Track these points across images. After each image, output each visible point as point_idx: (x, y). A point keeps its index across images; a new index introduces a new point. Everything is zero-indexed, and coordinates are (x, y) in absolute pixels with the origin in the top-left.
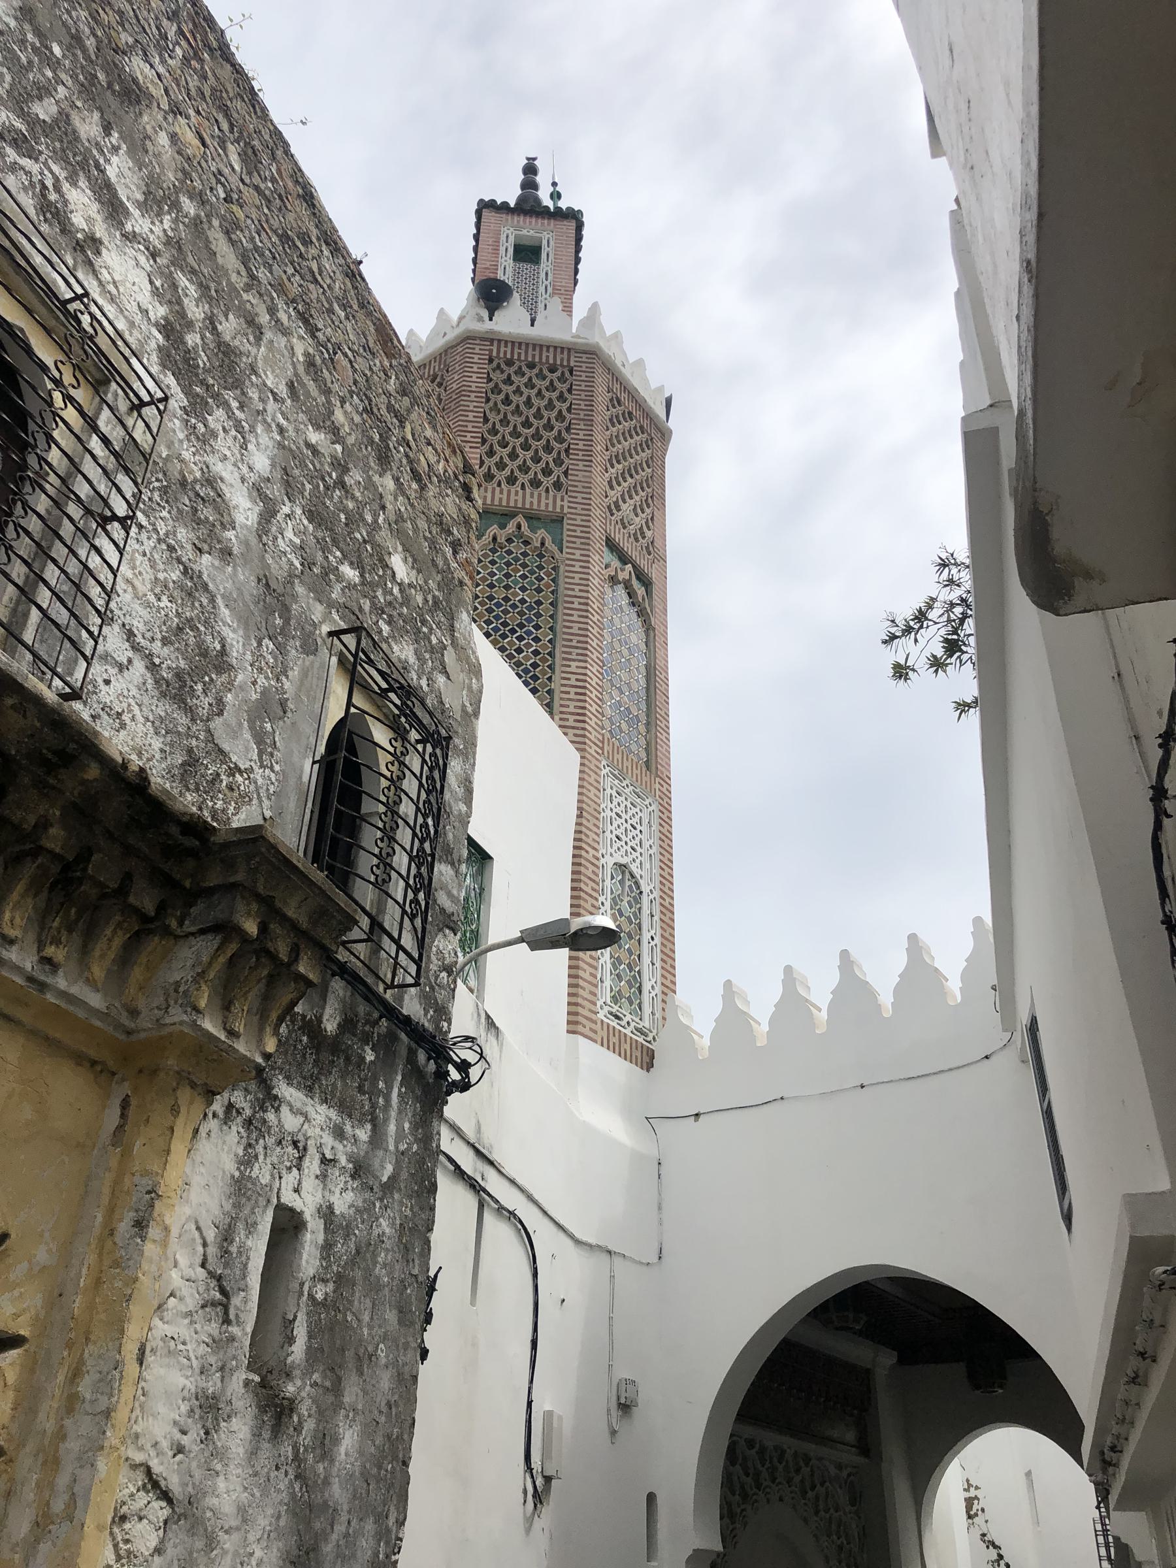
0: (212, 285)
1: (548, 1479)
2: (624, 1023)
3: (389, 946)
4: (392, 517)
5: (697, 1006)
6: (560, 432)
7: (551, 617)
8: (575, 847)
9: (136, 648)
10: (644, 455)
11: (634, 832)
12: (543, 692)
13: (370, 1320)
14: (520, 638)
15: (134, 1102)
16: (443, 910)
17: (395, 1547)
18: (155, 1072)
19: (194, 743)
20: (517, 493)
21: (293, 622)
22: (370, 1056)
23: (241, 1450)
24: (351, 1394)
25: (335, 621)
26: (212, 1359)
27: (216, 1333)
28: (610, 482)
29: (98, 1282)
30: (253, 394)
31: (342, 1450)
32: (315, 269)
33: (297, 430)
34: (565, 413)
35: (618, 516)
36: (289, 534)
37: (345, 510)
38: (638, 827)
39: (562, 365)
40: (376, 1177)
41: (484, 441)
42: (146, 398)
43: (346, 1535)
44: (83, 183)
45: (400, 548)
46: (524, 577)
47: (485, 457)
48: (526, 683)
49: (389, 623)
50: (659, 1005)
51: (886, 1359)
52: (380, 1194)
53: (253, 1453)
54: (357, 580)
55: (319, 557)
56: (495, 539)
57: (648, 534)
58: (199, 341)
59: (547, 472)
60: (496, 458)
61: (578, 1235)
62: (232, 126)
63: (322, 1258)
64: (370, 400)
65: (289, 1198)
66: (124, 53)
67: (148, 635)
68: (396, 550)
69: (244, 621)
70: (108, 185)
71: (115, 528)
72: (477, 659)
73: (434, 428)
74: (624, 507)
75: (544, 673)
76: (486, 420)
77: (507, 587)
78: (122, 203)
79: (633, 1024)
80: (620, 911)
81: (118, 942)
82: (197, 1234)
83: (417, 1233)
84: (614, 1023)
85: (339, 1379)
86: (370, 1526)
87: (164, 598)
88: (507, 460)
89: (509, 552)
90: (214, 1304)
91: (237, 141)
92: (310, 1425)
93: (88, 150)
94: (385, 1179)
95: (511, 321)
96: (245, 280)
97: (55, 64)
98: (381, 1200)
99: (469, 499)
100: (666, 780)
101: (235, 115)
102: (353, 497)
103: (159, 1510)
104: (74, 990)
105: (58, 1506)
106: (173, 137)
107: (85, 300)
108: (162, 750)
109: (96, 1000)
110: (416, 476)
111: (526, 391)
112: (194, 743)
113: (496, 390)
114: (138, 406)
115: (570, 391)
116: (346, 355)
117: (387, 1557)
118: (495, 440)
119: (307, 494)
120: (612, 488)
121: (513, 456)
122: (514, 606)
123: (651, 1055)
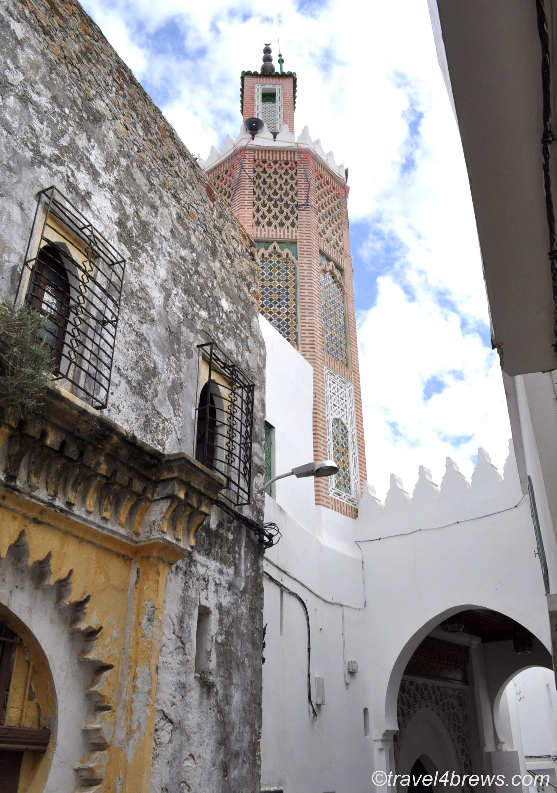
0: (136, 195)
1: (319, 706)
2: (342, 497)
3: (234, 488)
4: (220, 281)
5: (378, 486)
6: (292, 196)
7: (294, 294)
8: (314, 413)
9: (121, 375)
10: (336, 202)
11: (342, 401)
12: (292, 336)
13: (240, 648)
14: (279, 307)
15: (141, 571)
16: (256, 465)
17: (259, 736)
18: (148, 558)
19: (147, 412)
20: (272, 231)
21: (182, 345)
22: (231, 537)
23: (196, 703)
24: (236, 679)
25: (199, 339)
26: (182, 669)
27: (181, 659)
28: (319, 220)
29: (137, 643)
30: (156, 241)
31: (234, 701)
32: (178, 170)
33: (176, 252)
34: (294, 186)
35: (324, 237)
36: (177, 303)
37: (199, 284)
38: (344, 398)
39: (291, 161)
40: (238, 589)
41: (254, 204)
42: (115, 261)
43: (239, 732)
44: (82, 168)
45: (224, 295)
46: (279, 274)
47: (255, 213)
48: (284, 336)
49: (222, 333)
50: (359, 486)
51: (475, 642)
52: (240, 596)
53: (201, 704)
54: (207, 316)
55: (190, 310)
56: (263, 255)
57: (341, 244)
58: (132, 224)
59: (287, 218)
60: (261, 213)
61: (326, 599)
62: (137, 115)
63: (219, 625)
64: (206, 226)
65: (204, 602)
66: (92, 100)
67: (126, 368)
68: (223, 297)
69: (161, 350)
70: (92, 166)
71: (109, 326)
72: (263, 339)
73: (235, 229)
74: (327, 232)
75: (292, 324)
76: (254, 193)
77: (271, 280)
78: (97, 171)
79: (347, 497)
80: (337, 442)
81: (130, 505)
82: (170, 620)
83: (256, 611)
84: (337, 498)
85: (231, 674)
86: (248, 729)
87: (130, 349)
88: (266, 213)
89: (271, 262)
90: (179, 648)
91: (140, 121)
92: (221, 692)
93: (83, 152)
94: (241, 589)
95: (264, 139)
96: (149, 187)
97: (65, 117)
98: (241, 598)
99: (254, 260)
100: (357, 373)
101: (139, 109)
102: (203, 277)
103: (169, 727)
104: (115, 528)
105: (134, 727)
106: (115, 132)
107: (89, 228)
108: (136, 418)
109: (122, 531)
110: (229, 256)
111: (274, 176)
112: (147, 412)
113: (259, 177)
114: (111, 265)
115: (296, 174)
116: (194, 207)
117: (256, 740)
118: (259, 203)
119: (182, 282)
120: (320, 222)
121: (269, 211)
122: (275, 290)
123: (356, 511)
